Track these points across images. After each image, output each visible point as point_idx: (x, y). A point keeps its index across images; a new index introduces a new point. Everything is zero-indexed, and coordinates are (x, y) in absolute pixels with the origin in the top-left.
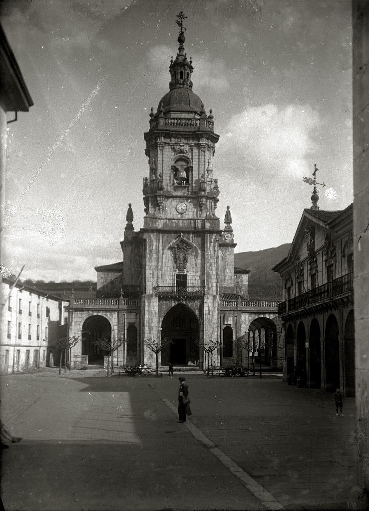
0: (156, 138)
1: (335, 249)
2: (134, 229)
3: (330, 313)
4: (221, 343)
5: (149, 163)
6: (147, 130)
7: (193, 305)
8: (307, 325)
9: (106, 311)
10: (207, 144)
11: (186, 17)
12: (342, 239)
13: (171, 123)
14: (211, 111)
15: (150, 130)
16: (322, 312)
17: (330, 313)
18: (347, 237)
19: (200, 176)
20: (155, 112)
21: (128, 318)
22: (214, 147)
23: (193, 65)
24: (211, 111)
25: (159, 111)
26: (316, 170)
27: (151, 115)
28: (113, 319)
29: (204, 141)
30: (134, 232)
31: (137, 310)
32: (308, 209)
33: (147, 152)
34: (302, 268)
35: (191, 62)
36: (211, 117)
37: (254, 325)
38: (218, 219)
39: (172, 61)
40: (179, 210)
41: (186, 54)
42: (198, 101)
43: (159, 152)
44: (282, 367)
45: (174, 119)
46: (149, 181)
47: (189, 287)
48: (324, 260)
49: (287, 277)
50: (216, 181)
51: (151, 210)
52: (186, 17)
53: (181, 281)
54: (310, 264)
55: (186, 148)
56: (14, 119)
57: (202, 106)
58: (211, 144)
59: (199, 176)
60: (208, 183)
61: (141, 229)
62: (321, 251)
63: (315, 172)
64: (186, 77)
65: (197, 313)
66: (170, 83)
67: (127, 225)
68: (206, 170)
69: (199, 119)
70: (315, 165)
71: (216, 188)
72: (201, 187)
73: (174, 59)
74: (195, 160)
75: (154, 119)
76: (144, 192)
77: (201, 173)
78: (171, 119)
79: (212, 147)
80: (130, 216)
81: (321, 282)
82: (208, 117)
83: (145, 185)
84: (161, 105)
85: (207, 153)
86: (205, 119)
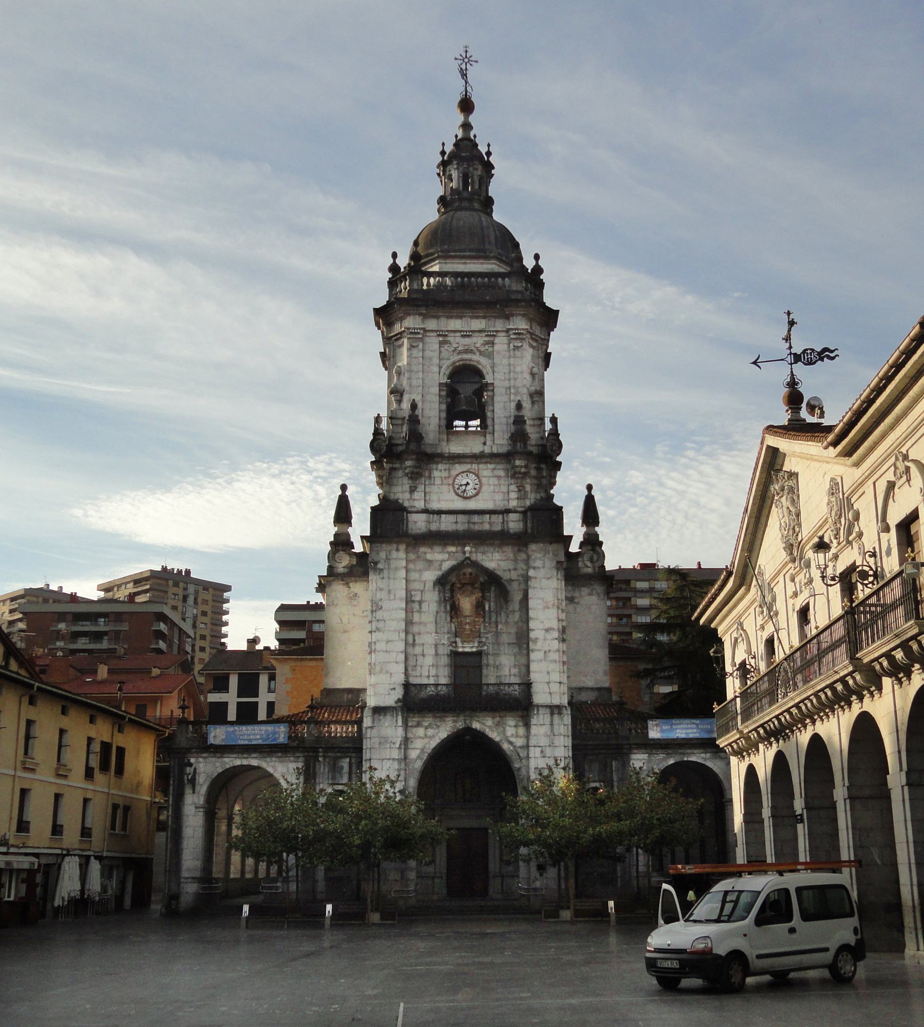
1: (857, 517)
3: (856, 709)
7: (504, 732)
11: (476, 62)
12: (874, 483)
14: (537, 257)
16: (833, 711)
17: (856, 709)
18: (893, 468)
23: (492, 159)
24: (537, 257)
26: (792, 323)
30: (355, 553)
35: (489, 154)
36: (538, 270)
39: (443, 153)
44: (407, 553)
49: (735, 635)
52: (476, 62)
54: (793, 580)
55: (478, 341)
56: (715, 917)
67: (336, 535)
70: (789, 313)
71: (555, 433)
74: (501, 361)
76: (373, 447)
83: (377, 432)
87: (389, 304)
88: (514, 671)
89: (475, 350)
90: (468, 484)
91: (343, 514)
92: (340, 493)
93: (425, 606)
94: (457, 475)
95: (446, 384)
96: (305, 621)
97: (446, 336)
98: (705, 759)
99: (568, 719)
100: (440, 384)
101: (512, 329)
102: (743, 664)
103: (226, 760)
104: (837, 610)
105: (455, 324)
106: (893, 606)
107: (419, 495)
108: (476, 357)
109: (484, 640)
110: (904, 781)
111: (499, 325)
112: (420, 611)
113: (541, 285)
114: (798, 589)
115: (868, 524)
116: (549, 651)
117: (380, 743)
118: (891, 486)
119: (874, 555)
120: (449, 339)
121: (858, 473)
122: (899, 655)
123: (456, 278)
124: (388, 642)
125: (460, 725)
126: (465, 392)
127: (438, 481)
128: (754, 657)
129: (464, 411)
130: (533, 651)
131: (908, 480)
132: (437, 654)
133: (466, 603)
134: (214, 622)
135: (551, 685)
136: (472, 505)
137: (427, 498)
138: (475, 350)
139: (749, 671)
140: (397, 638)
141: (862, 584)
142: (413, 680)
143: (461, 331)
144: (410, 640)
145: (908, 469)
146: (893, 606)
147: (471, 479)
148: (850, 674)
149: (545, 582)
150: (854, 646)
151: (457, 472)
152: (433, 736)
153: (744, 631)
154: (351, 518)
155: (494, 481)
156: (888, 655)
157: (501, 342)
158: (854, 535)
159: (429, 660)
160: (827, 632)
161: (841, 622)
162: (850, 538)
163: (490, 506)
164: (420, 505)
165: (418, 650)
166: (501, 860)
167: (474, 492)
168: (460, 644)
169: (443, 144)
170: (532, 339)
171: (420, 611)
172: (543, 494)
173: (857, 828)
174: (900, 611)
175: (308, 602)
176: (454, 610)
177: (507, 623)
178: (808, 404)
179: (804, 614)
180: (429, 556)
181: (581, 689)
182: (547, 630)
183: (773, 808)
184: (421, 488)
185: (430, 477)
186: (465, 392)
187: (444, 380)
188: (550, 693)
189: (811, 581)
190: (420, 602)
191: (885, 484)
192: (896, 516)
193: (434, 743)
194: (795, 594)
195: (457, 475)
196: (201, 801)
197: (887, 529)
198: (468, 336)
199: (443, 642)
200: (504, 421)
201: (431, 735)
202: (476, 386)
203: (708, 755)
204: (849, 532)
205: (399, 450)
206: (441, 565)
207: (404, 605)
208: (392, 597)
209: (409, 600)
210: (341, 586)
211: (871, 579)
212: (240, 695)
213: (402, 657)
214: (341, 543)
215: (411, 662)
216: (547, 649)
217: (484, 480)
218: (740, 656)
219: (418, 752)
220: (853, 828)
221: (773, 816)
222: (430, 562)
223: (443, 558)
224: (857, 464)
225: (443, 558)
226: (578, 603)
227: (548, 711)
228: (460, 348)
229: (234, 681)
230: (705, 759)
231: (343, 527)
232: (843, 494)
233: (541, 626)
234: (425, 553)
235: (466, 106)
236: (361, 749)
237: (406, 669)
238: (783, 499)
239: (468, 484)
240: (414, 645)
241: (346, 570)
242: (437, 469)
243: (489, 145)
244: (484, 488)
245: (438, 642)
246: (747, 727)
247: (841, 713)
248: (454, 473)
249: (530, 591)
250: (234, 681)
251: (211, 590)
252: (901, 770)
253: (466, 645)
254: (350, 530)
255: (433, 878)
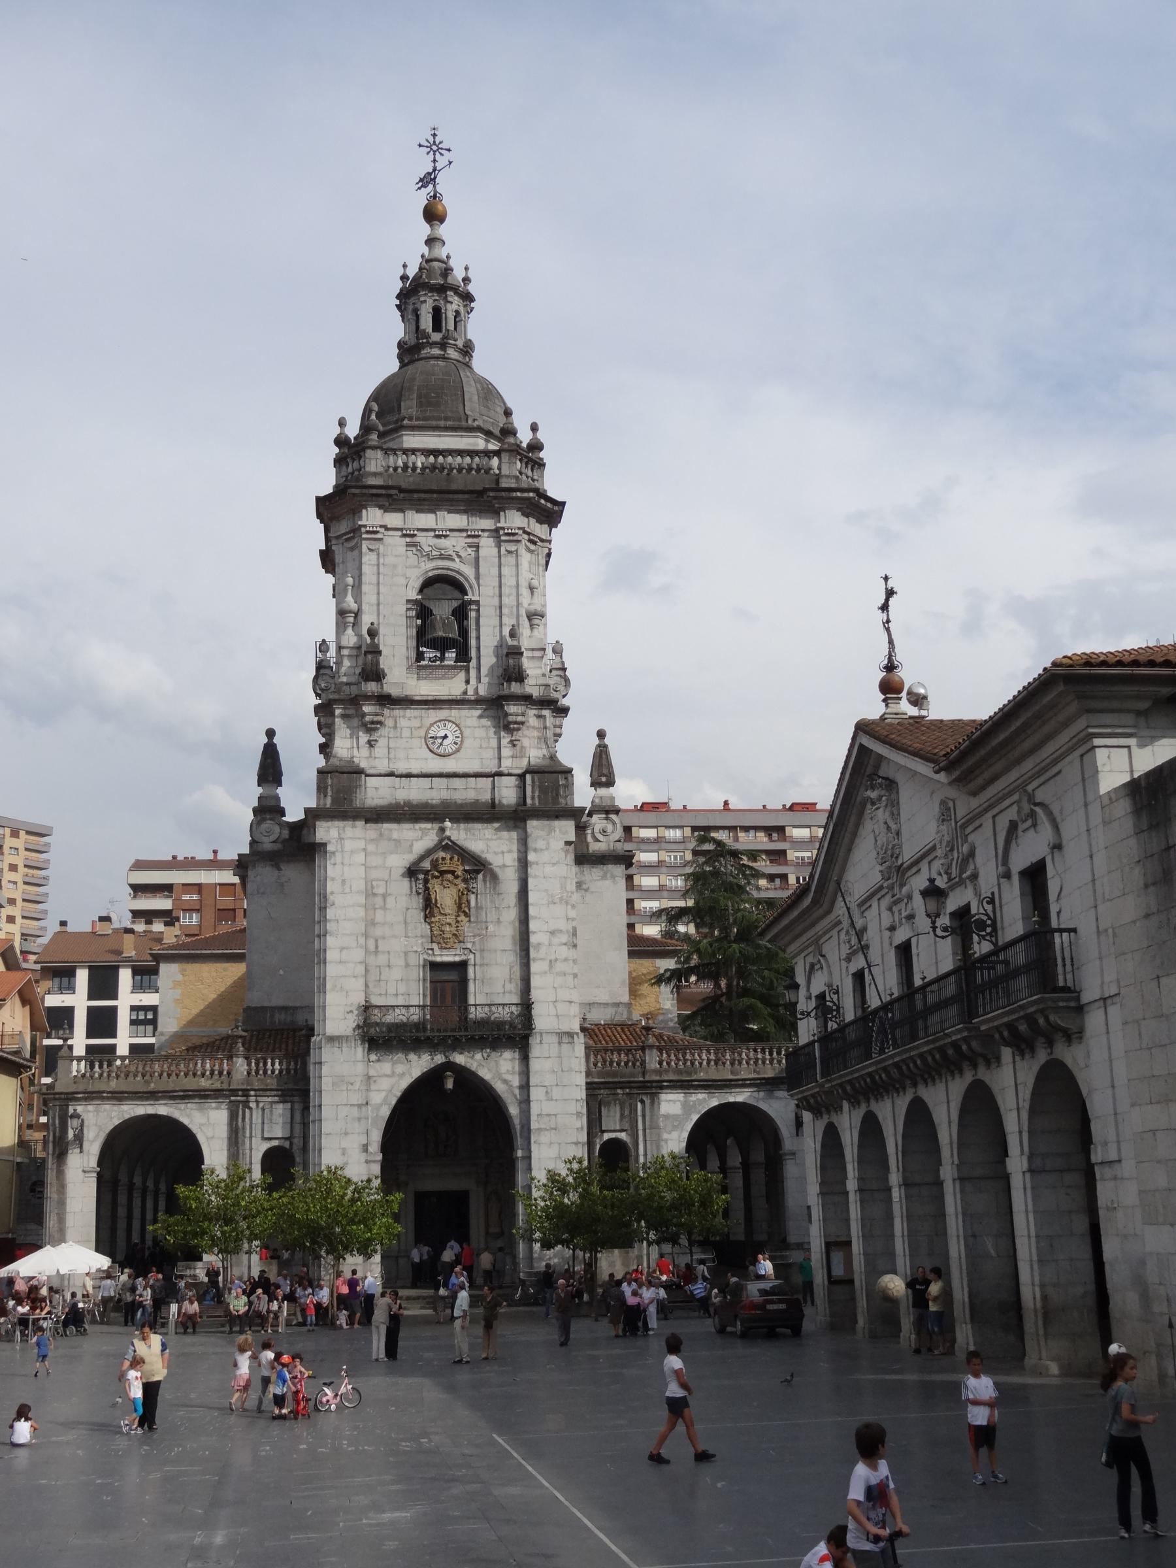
0: (356, 512)
1: (972, 854)
2: (282, 812)
4: (319, 963)
5: (334, 596)
6: (327, 488)
7: (496, 1069)
8: (945, 1120)
9: (186, 1096)
10: (525, 532)
11: (449, 150)
13: (405, 467)
14: (534, 428)
15: (336, 487)
16: (940, 1075)
18: (1015, 807)
19: (506, 631)
20: (352, 431)
21: (269, 1125)
22: (550, 542)
24: (534, 428)
25: (366, 428)
26: (890, 593)
27: (341, 441)
28: (208, 1125)
29: (514, 520)
31: (298, 1091)
32: (874, 722)
33: (328, 560)
34: (965, 849)
35: (466, 280)
36: (536, 446)
37: (708, 1134)
38: (569, 771)
39: (404, 278)
40: (431, 746)
41: (448, 257)
42: (489, 393)
43: (368, 559)
45: (414, 451)
46: (332, 653)
47: (475, 1005)
48: (844, 956)
49: (810, 959)
50: (558, 650)
51: (343, 746)
53: (448, 980)
54: (890, 909)
57: (508, 413)
58: (540, 530)
59: (501, 631)
60: (530, 654)
61: (307, 811)
62: (989, 815)
63: (887, 600)
64: (451, 327)
65: (514, 1110)
66: (400, 345)
68: (523, 612)
69: (497, 453)
70: (886, 578)
72: (510, 668)
73: (412, 272)
74: (488, 569)
75: (349, 452)
77: (508, 622)
78: (406, 452)
79: (542, 541)
80: (270, 768)
81: (933, 969)
82: (524, 445)
84: (371, 411)
85: (525, 558)
86: (516, 450)
87: (340, 491)
88: (509, 987)
89: (454, 555)
90: (445, 737)
91: (270, 768)
92: (266, 740)
93: (390, 901)
94: (432, 725)
95: (415, 602)
96: (172, 885)
97: (414, 535)
98: (758, 1099)
99: (580, 1050)
100: (408, 601)
101: (503, 528)
102: (821, 997)
103: (125, 1108)
104: (947, 964)
105: (425, 520)
106: (1015, 973)
107: (380, 750)
108: (457, 565)
109: (469, 946)
110: (1025, 1166)
111: (487, 523)
112: (384, 908)
113: (540, 465)
114: (897, 919)
115: (987, 867)
116: (556, 960)
117: (333, 1084)
118: (1013, 827)
119: (992, 901)
120: (417, 539)
121: (975, 803)
122: (1023, 1027)
123: (427, 456)
124: (342, 949)
125: (439, 1059)
126: (444, 619)
127: (406, 733)
128: (837, 992)
129: (442, 638)
130: (534, 960)
131: (1034, 825)
132: (407, 965)
133: (446, 897)
134: (27, 880)
135: (559, 1005)
136: (450, 765)
137: (392, 756)
138: (454, 555)
139: (830, 1010)
140: (354, 945)
141: (978, 935)
142: (376, 1001)
143: (434, 530)
144: (372, 947)
145: (1032, 814)
146: (1015, 973)
147: (450, 730)
148: (965, 1039)
149: (549, 869)
150: (970, 1013)
151: (432, 720)
152: (403, 1074)
153: (823, 956)
154: (280, 774)
155: (480, 733)
156: (1010, 1026)
157: (487, 544)
158: (968, 873)
159: (397, 973)
160: (935, 987)
161: (952, 979)
162: (964, 876)
163: (475, 767)
164: (382, 766)
165: (382, 959)
166: (487, 1233)
167: (454, 747)
168: (437, 951)
169: (405, 266)
170: (530, 541)
171: (384, 908)
172: (545, 751)
173: (967, 1215)
174: (1022, 982)
175: (174, 857)
176: (429, 907)
177: (499, 921)
178: (909, 693)
179: (905, 951)
180: (395, 835)
181: (590, 1005)
182: (552, 933)
183: (861, 1179)
184: (382, 742)
185: (395, 727)
186: (444, 619)
187: (414, 595)
188: (557, 1016)
189: (911, 917)
190: (384, 896)
191: (1007, 824)
192: (1021, 859)
193: (405, 1083)
194: (892, 929)
195: (432, 725)
196: (93, 1162)
197: (1007, 875)
198: (445, 536)
199: (415, 948)
200: (491, 650)
201: (403, 1071)
202: (455, 604)
203: (762, 1094)
204: (963, 870)
205: (349, 691)
206: (411, 846)
207: (363, 901)
208: (347, 890)
209: (370, 893)
210: (268, 869)
211: (989, 930)
212: (91, 997)
213: (361, 969)
214: (268, 810)
215: (373, 976)
216: (553, 958)
217: (467, 732)
218: (818, 985)
219: (384, 1094)
220: (964, 1214)
221: (860, 1190)
222: (398, 842)
223: (419, 838)
224: (974, 794)
225: (419, 838)
226: (586, 890)
227: (555, 1039)
228: (434, 553)
229: (82, 977)
230: (758, 1099)
231: (269, 790)
232: (956, 823)
233: (545, 928)
234: (391, 830)
235: (433, 215)
236: (308, 1091)
237: (367, 986)
238: (880, 813)
239: (445, 737)
240: (376, 952)
241: (278, 846)
242: (404, 717)
243: (466, 269)
244: (467, 743)
245: (409, 949)
246: (830, 1081)
247: (949, 1078)
248: (427, 722)
249: (530, 881)
250: (82, 977)
251: (22, 833)
252: (1022, 1154)
253: (445, 952)
254: (280, 791)
255: (397, 1258)
